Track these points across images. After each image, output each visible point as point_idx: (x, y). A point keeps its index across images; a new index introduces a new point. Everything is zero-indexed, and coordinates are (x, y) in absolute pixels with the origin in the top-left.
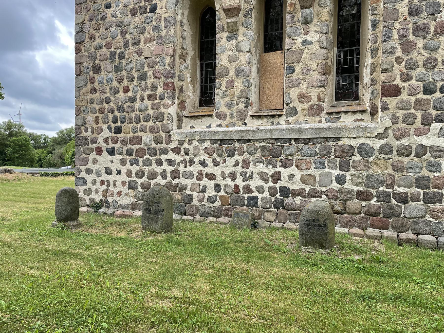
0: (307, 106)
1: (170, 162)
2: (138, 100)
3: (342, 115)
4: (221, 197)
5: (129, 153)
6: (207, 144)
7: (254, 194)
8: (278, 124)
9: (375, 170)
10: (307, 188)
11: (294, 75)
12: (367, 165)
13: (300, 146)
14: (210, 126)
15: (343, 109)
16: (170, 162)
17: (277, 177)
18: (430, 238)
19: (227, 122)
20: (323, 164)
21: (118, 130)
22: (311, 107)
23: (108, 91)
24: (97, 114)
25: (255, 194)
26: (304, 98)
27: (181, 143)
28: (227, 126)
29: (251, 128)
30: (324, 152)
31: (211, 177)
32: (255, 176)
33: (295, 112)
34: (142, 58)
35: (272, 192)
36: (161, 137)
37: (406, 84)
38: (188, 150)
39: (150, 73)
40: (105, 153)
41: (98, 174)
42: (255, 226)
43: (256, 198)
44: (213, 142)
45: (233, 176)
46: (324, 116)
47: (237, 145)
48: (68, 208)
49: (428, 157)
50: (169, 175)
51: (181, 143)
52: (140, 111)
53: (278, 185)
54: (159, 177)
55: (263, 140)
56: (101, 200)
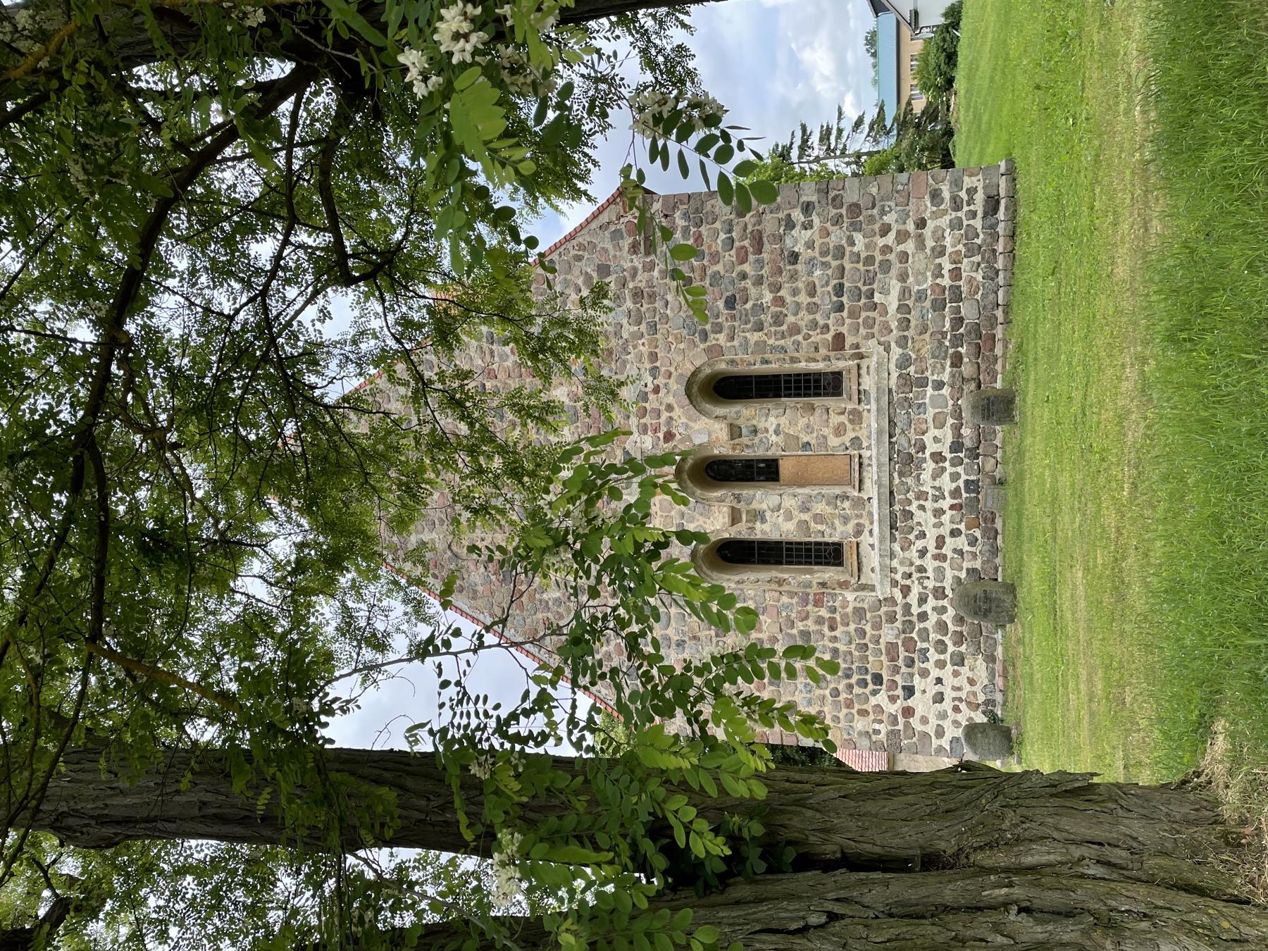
0: (849, 426)
1: (922, 600)
2: (836, 645)
3: (862, 388)
4: (968, 528)
5: (910, 663)
6: (897, 547)
7: (962, 485)
8: (870, 458)
9: (926, 350)
10: (950, 421)
11: (813, 442)
12: (920, 359)
13: (898, 431)
14: (872, 546)
15: (855, 387)
16: (922, 600)
17: (938, 457)
18: (1001, 293)
19: (867, 523)
20: (920, 406)
21: (878, 679)
22: (851, 421)
23: (821, 692)
24: (854, 711)
25: (961, 483)
26: (840, 430)
27: (894, 583)
28: (872, 523)
29: (876, 489)
30: (906, 404)
31: (940, 542)
32: (937, 484)
33: (856, 441)
34: (780, 637)
35: (957, 462)
36: (886, 613)
37: (832, 328)
38: (904, 573)
39: (800, 625)
40: (910, 702)
41: (943, 715)
42: (1001, 483)
43: (967, 482)
44: (893, 539)
45: (938, 513)
46: (863, 406)
47: (897, 507)
48: (991, 734)
49: (910, 303)
50: (940, 603)
51: (894, 583)
52: (850, 643)
53: (949, 456)
54: (944, 617)
55: (891, 475)
56: (984, 713)
